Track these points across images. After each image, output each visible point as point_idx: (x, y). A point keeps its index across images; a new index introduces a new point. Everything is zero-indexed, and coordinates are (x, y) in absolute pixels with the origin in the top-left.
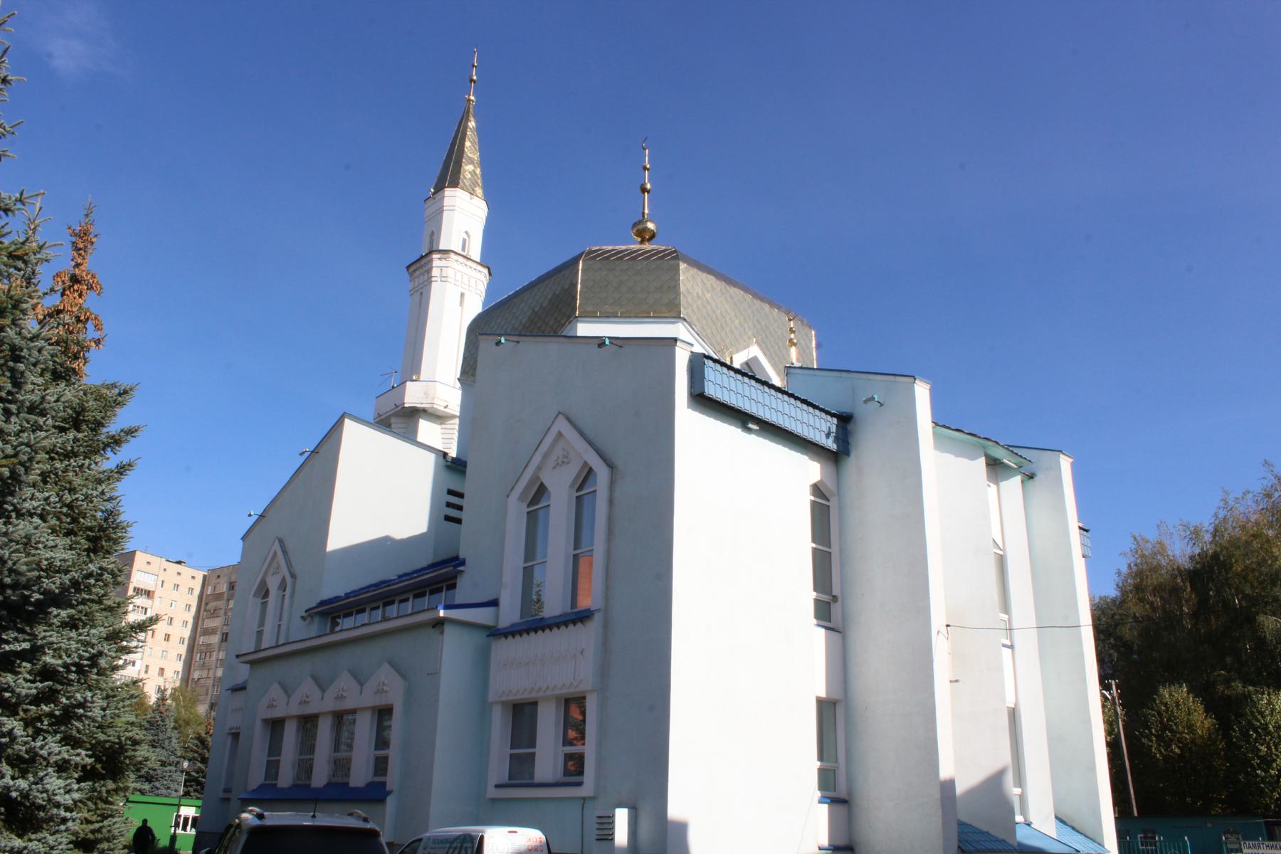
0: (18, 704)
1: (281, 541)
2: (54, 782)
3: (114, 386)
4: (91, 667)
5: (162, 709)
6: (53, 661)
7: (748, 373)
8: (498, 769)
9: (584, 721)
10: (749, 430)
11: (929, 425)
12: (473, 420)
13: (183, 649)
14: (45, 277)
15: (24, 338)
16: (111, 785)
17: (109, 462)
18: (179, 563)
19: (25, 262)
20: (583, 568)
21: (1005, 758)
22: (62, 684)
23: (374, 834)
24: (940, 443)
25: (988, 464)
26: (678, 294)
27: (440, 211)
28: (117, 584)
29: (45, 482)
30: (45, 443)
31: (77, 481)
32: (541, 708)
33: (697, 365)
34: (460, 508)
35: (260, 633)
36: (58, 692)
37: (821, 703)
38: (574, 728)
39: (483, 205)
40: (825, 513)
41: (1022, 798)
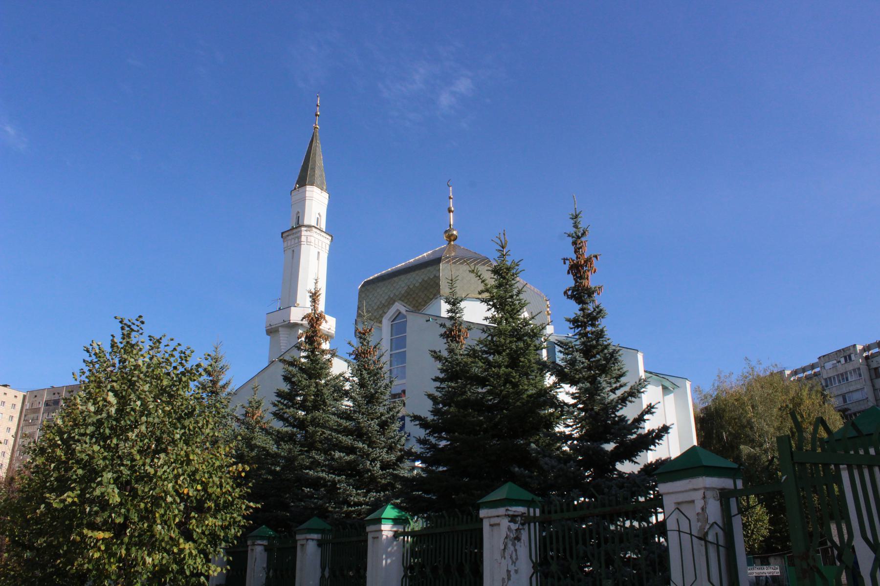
18: (5, 386)
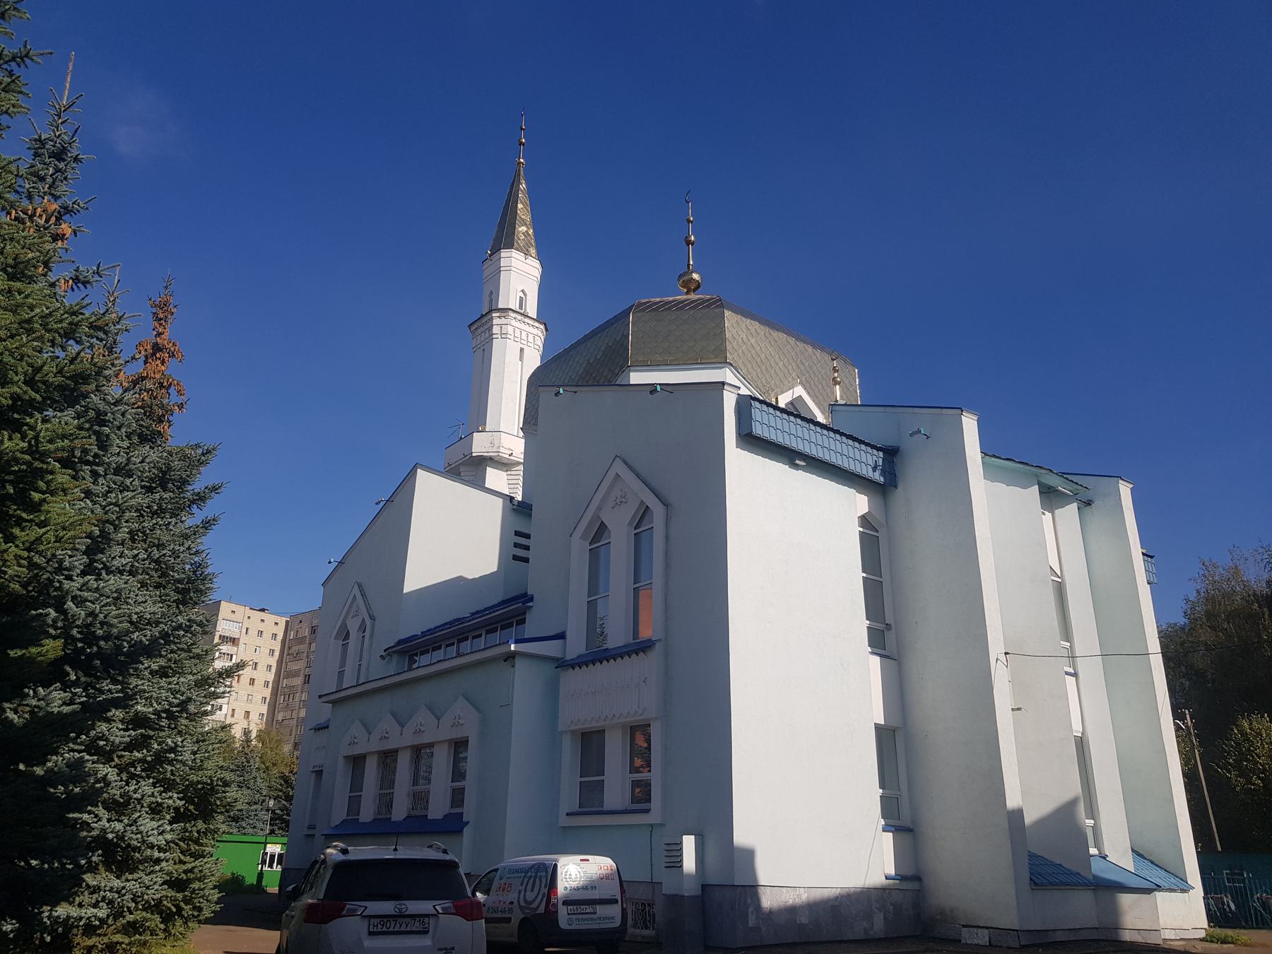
0: (112, 752)
1: (360, 586)
2: (148, 824)
3: (198, 446)
4: (181, 712)
5: (246, 750)
6: (145, 709)
7: (794, 412)
8: (569, 797)
9: (649, 748)
10: (796, 467)
11: (979, 455)
12: (537, 462)
13: (267, 693)
14: (126, 347)
15: (108, 403)
16: (201, 825)
17: (191, 520)
18: (263, 610)
19: (106, 333)
20: (642, 601)
21: (1075, 789)
22: (154, 729)
23: (453, 865)
24: (990, 473)
25: (1041, 493)
26: (724, 340)
27: (498, 271)
28: (205, 633)
29: (133, 541)
30: (133, 502)
31: (164, 539)
32: (608, 737)
33: (744, 406)
34: (527, 548)
35: (341, 673)
36: (151, 737)
37: (878, 728)
38: (640, 756)
39: (537, 264)
40: (875, 543)
41: (1096, 829)
